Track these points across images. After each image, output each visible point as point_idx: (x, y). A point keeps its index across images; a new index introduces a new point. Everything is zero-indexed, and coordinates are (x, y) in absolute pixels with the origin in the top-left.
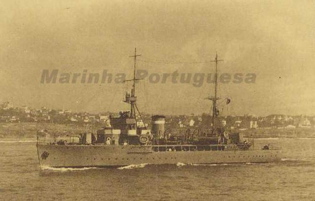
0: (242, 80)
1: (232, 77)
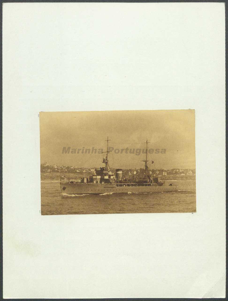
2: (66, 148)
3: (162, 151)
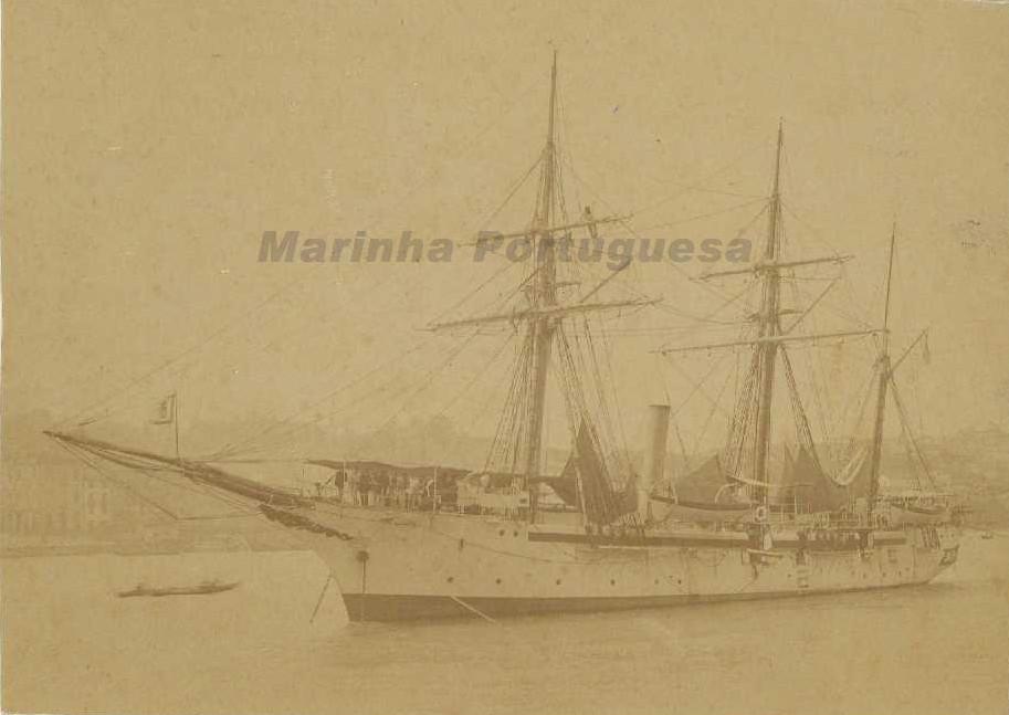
1: (698, 251)
2: (278, 234)
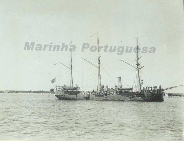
0: (149, 51)
2: (29, 43)
3: (36, 47)
